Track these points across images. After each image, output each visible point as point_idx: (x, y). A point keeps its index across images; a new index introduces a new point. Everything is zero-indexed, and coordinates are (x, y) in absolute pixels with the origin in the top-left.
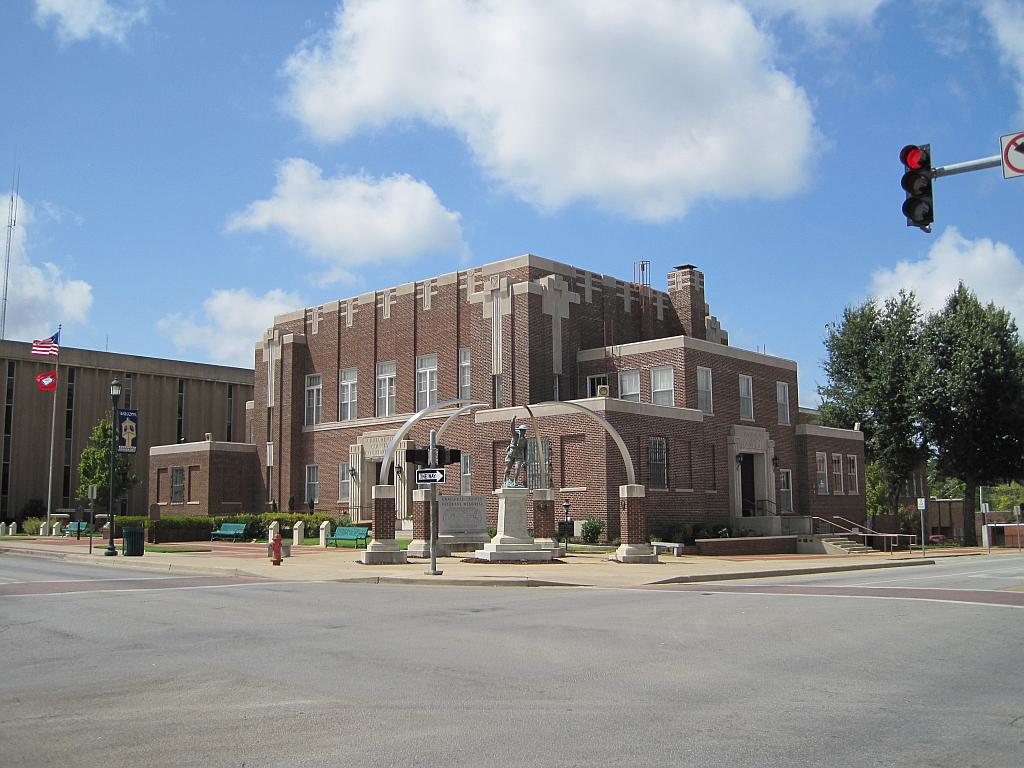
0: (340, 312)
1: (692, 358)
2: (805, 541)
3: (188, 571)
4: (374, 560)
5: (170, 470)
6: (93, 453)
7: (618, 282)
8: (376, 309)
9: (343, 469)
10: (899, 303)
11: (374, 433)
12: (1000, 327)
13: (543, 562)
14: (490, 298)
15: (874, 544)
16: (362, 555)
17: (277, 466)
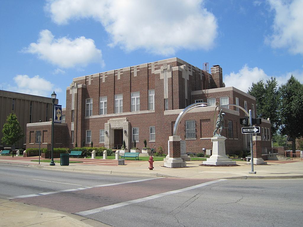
7: (199, 70)
8: (115, 76)
11: (114, 119)
14: (163, 72)
17: (75, 131)
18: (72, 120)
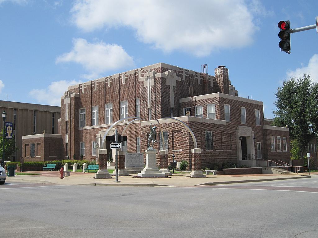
0: (92, 85)
1: (222, 101)
2: (265, 169)
3: (28, 182)
4: (99, 177)
7: (196, 73)
9: (94, 143)
13: (162, 177)
15: (292, 170)
16: (95, 175)
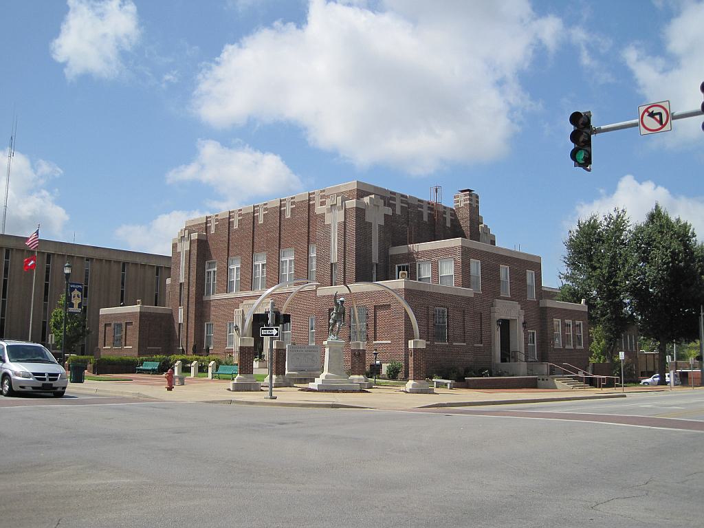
1: (467, 253)
2: (543, 380)
4: (238, 388)
5: (112, 325)
6: (58, 312)
7: (419, 201)
8: (254, 217)
9: (230, 325)
10: (615, 217)
12: (683, 234)
15: (592, 383)
16: (230, 385)
17: (185, 324)
18: (180, 302)
